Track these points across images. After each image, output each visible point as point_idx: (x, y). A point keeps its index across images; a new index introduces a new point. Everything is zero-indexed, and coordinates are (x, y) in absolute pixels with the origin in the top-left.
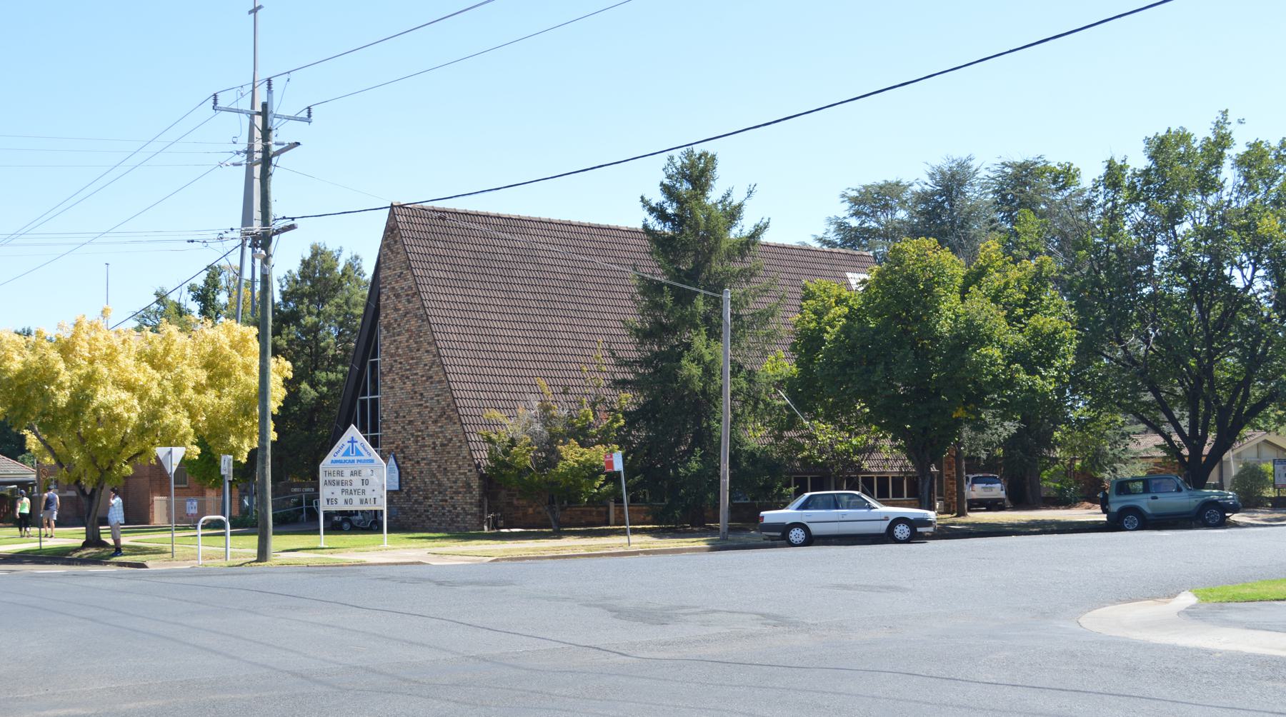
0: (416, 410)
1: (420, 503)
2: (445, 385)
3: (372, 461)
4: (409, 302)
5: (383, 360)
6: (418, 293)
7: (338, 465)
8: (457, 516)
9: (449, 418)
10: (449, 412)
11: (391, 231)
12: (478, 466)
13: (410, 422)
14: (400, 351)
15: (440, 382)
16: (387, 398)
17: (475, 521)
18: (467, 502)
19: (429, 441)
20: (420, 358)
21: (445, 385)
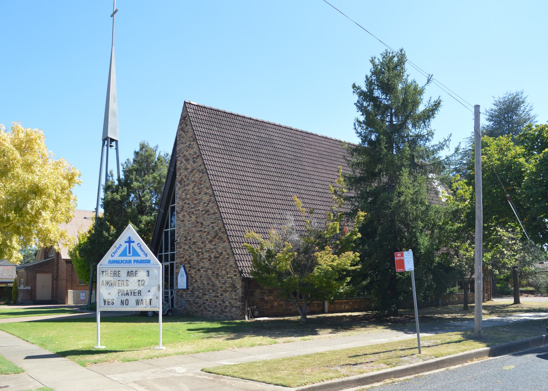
0: (198, 234)
1: (200, 298)
2: (218, 215)
3: (148, 261)
4: (194, 162)
5: (178, 204)
6: (200, 155)
7: (115, 265)
8: (226, 308)
9: (221, 238)
10: (221, 234)
11: (184, 118)
12: (241, 272)
13: (194, 243)
14: (188, 196)
15: (214, 213)
16: (180, 228)
17: (239, 312)
18: (233, 298)
19: (206, 255)
20: (201, 199)
21: (218, 215)
